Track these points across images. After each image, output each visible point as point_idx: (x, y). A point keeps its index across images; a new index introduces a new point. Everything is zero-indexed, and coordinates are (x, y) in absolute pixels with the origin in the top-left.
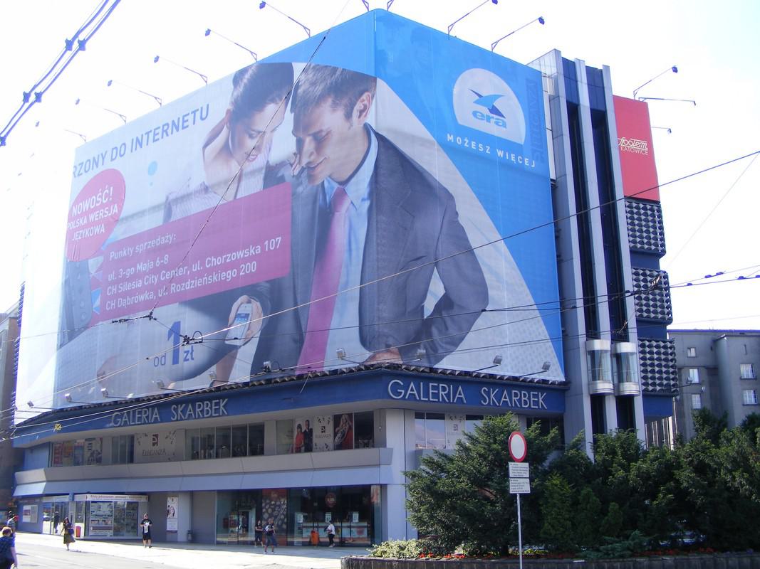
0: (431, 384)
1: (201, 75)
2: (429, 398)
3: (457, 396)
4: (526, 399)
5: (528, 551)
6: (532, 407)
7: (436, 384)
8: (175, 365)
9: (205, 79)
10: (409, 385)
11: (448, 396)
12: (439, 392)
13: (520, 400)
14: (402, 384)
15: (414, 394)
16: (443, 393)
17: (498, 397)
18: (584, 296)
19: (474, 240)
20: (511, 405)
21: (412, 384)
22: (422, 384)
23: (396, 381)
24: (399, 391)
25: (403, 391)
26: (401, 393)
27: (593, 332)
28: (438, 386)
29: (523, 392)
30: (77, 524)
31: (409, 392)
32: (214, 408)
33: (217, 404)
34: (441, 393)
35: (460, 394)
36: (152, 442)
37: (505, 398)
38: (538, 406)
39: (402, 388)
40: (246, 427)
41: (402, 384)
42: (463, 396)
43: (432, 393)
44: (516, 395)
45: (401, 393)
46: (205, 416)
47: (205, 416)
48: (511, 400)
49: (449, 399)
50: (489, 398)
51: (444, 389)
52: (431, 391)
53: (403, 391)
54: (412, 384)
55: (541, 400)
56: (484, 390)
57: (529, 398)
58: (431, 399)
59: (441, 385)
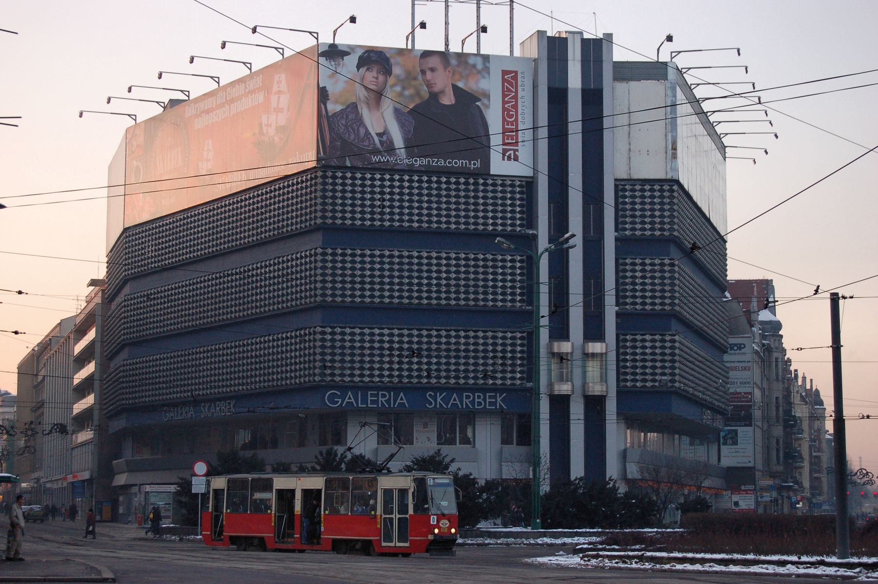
0: (369, 393)
2: (367, 404)
3: (398, 401)
4: (739, 384)
5: (400, 516)
6: (488, 407)
7: (493, 394)
10: (453, 395)
11: (388, 401)
12: (378, 399)
13: (473, 402)
16: (383, 399)
17: (446, 400)
20: (462, 406)
21: (350, 393)
23: (329, 393)
27: (560, 331)
28: (378, 394)
29: (476, 394)
30: (519, 169)
31: (347, 400)
32: (488, 400)
33: (229, 403)
34: (380, 399)
35: (455, 400)
37: (402, 399)
38: (496, 407)
39: (339, 397)
42: (405, 401)
44: (468, 397)
46: (512, 152)
47: (512, 152)
48: (461, 403)
49: (389, 404)
50: (436, 401)
51: (384, 396)
52: (369, 398)
53: (340, 400)
54: (350, 393)
55: (499, 400)
56: (430, 395)
57: (485, 400)
58: (369, 406)
59: (380, 393)
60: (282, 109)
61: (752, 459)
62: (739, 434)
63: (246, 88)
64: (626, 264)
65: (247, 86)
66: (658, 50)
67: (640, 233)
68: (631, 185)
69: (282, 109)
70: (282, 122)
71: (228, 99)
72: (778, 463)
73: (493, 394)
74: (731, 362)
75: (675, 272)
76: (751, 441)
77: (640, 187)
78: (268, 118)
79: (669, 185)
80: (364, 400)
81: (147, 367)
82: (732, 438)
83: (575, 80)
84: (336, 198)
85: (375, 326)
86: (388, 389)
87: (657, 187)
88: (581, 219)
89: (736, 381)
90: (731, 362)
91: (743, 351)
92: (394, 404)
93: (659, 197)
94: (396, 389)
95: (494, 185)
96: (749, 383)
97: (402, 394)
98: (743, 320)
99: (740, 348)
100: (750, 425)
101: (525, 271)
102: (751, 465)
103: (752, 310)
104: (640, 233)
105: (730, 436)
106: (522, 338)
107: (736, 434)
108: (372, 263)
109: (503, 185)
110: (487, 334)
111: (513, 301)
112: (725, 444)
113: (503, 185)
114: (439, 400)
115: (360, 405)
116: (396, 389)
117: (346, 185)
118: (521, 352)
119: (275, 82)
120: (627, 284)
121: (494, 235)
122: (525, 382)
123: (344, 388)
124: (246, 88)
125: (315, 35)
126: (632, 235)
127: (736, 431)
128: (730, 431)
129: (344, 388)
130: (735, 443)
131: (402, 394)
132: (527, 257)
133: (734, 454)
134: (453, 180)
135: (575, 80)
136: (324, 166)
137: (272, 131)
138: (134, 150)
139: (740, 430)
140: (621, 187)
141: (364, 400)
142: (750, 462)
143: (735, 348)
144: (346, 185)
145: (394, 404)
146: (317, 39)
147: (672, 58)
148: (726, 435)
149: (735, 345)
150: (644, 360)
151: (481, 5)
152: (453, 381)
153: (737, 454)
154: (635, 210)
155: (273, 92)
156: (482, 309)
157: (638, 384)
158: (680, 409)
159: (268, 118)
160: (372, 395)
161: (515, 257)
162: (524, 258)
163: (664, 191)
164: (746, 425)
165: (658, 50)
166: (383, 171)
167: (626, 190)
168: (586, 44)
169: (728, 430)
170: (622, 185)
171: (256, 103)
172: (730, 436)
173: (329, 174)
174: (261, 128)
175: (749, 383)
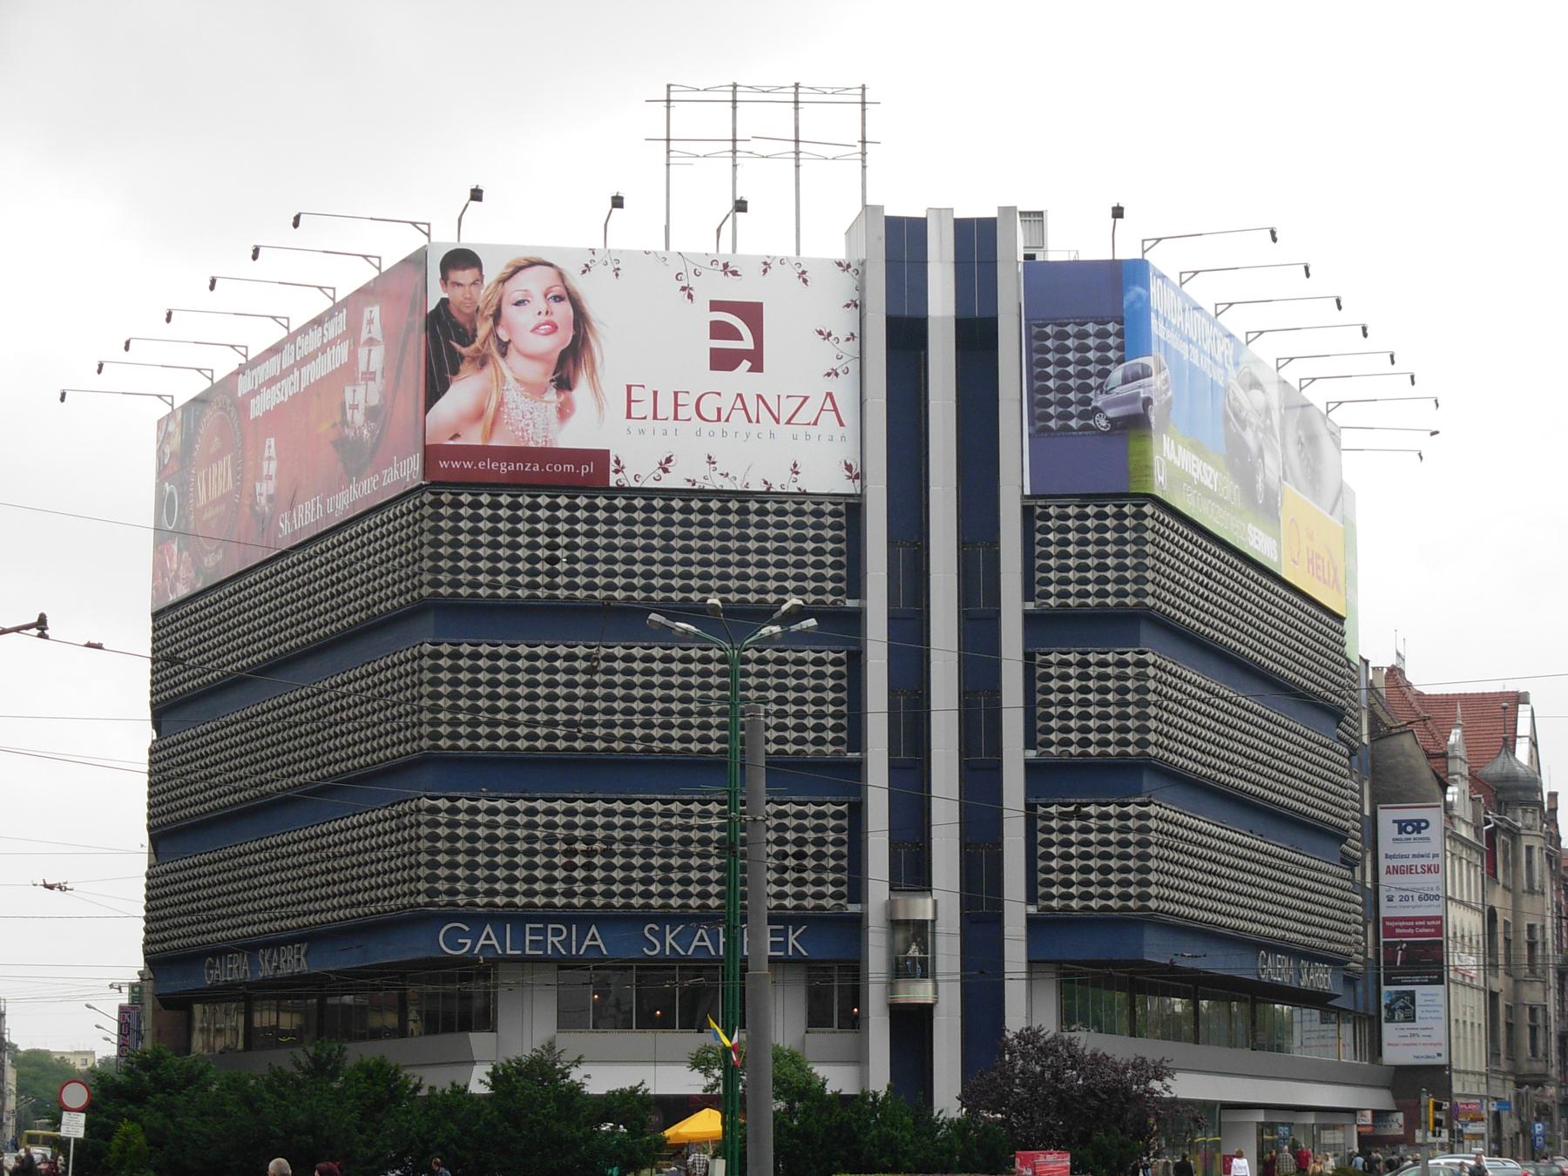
0: (528, 926)
1: (274, 318)
2: (524, 951)
3: (587, 942)
8: (1532, 923)
9: (285, 323)
11: (566, 944)
14: (467, 929)
15: (707, 947)
16: (555, 940)
18: (889, 786)
19: (1020, 713)
22: (508, 926)
24: (460, 941)
25: (469, 942)
26: (466, 944)
28: (546, 928)
31: (482, 941)
34: (550, 939)
36: (457, 1083)
39: (465, 935)
40: (637, 1028)
41: (467, 929)
42: (599, 942)
43: (531, 941)
45: (466, 944)
51: (558, 932)
52: (528, 938)
53: (469, 942)
55: (791, 939)
59: (550, 926)
60: (374, 373)
61: (1443, 1050)
62: (1419, 999)
63: (323, 335)
64: (1049, 664)
65: (325, 332)
66: (460, 220)
67: (585, 593)
68: (1059, 506)
69: (374, 373)
70: (374, 400)
71: (298, 358)
72: (1534, 1053)
73: (541, 926)
74: (1402, 857)
75: (1147, 677)
76: (1443, 1012)
77: (1077, 510)
78: (354, 391)
79: (1115, 506)
80: (518, 942)
81: (328, 884)
82: (1403, 1008)
83: (941, 302)
84: (460, 544)
85: (538, 795)
86: (567, 921)
87: (714, 505)
88: (884, 574)
89: (1410, 894)
90: (1402, 857)
91: (1424, 833)
92: (578, 949)
93: (1116, 529)
94: (580, 919)
95: (781, 512)
96: (1436, 897)
97: (593, 929)
98: (1424, 769)
99: (1418, 829)
100: (1440, 981)
101: (844, 682)
102: (1443, 1061)
103: (1450, 755)
104: (585, 593)
105: (1400, 1003)
106: (838, 815)
107: (1413, 1001)
108: (533, 670)
109: (799, 513)
110: (710, 807)
111: (819, 741)
112: (1390, 1019)
113: (799, 513)
114: (669, 939)
115: (509, 952)
116: (580, 919)
117: (479, 518)
118: (835, 843)
119: (365, 322)
120: (1051, 704)
121: (650, 606)
122: (842, 902)
123: (477, 920)
124: (323, 335)
125: (425, 228)
126: (1098, 605)
127: (1412, 994)
128: (1400, 995)
129: (477, 920)
130: (1411, 1018)
131: (593, 929)
132: (849, 654)
133: (1408, 1040)
134: (485, 499)
135: (941, 302)
136: (433, 484)
137: (359, 417)
138: (166, 462)
139: (1420, 991)
140: (1039, 510)
141: (518, 942)
142: (1439, 1055)
143: (1409, 829)
144: (479, 518)
145: (578, 949)
146: (428, 235)
147: (1144, 252)
148: (1393, 1002)
149: (1410, 822)
150: (1086, 856)
151: (801, 162)
152: (694, 902)
153: (1413, 1040)
154: (1068, 556)
155: (362, 341)
156: (660, 756)
157: (1074, 904)
158: (1157, 950)
159: (354, 391)
160: (533, 932)
161: (823, 655)
162: (843, 655)
163: (1125, 516)
164: (1431, 982)
165: (460, 220)
166: (476, 486)
167: (1048, 517)
168: (964, 228)
169: (1397, 992)
170: (1041, 507)
171: (338, 365)
172: (1400, 1003)
173: (446, 498)
174: (344, 413)
175: (1436, 897)
